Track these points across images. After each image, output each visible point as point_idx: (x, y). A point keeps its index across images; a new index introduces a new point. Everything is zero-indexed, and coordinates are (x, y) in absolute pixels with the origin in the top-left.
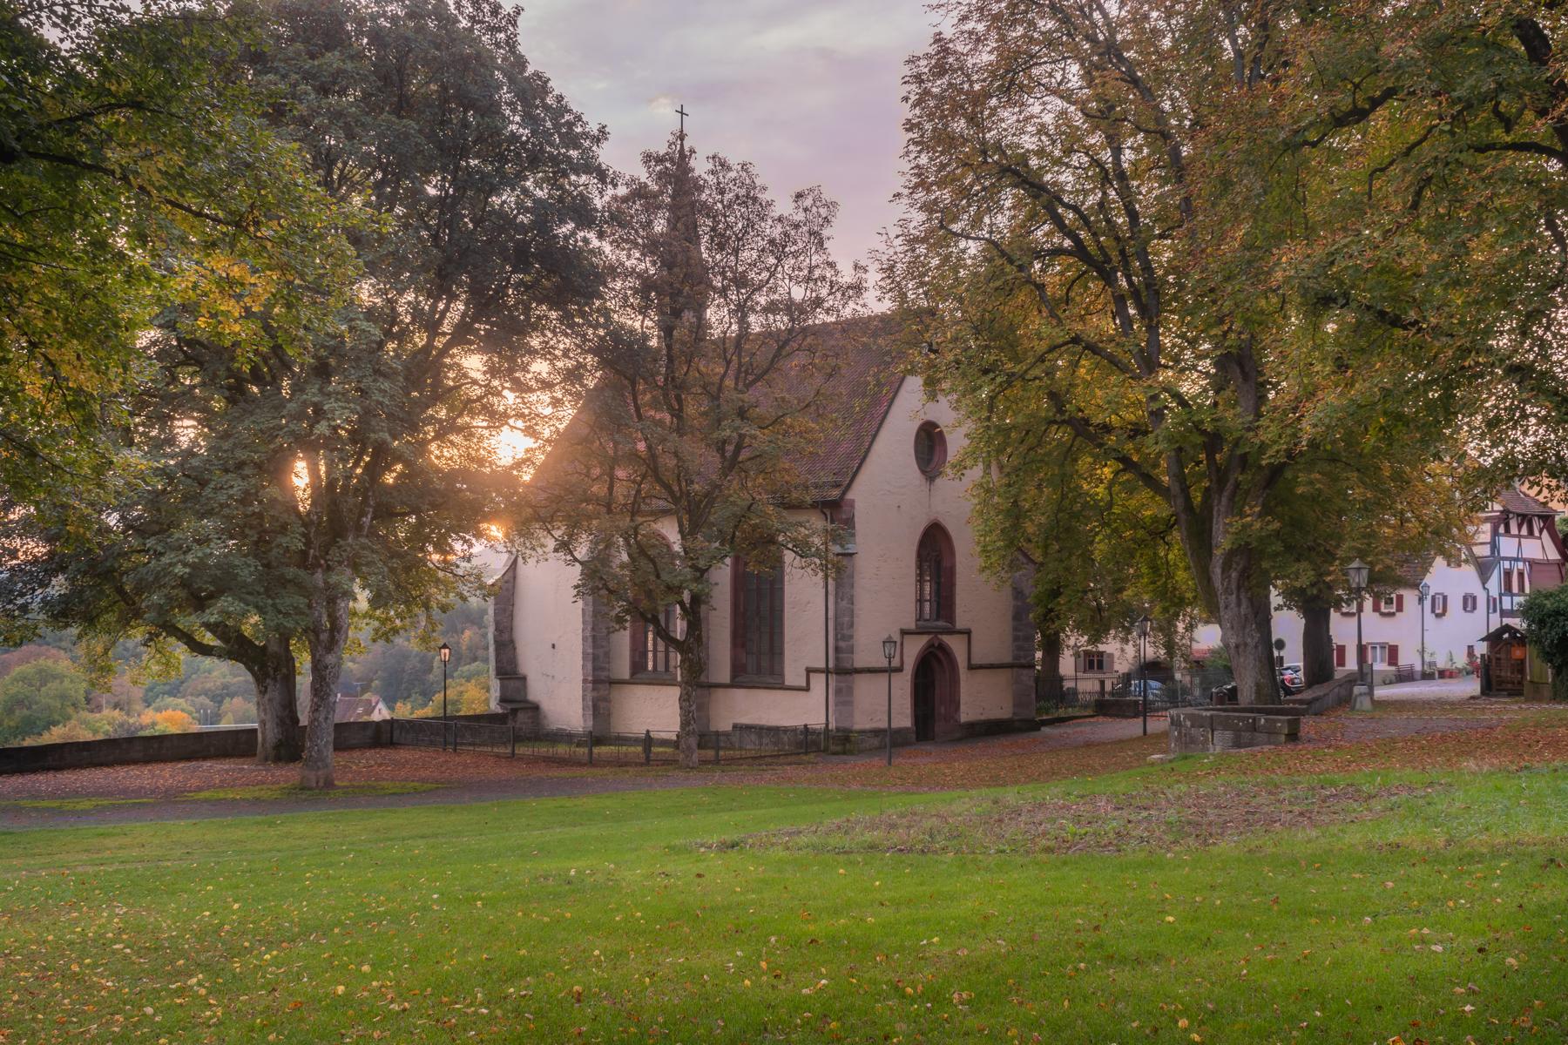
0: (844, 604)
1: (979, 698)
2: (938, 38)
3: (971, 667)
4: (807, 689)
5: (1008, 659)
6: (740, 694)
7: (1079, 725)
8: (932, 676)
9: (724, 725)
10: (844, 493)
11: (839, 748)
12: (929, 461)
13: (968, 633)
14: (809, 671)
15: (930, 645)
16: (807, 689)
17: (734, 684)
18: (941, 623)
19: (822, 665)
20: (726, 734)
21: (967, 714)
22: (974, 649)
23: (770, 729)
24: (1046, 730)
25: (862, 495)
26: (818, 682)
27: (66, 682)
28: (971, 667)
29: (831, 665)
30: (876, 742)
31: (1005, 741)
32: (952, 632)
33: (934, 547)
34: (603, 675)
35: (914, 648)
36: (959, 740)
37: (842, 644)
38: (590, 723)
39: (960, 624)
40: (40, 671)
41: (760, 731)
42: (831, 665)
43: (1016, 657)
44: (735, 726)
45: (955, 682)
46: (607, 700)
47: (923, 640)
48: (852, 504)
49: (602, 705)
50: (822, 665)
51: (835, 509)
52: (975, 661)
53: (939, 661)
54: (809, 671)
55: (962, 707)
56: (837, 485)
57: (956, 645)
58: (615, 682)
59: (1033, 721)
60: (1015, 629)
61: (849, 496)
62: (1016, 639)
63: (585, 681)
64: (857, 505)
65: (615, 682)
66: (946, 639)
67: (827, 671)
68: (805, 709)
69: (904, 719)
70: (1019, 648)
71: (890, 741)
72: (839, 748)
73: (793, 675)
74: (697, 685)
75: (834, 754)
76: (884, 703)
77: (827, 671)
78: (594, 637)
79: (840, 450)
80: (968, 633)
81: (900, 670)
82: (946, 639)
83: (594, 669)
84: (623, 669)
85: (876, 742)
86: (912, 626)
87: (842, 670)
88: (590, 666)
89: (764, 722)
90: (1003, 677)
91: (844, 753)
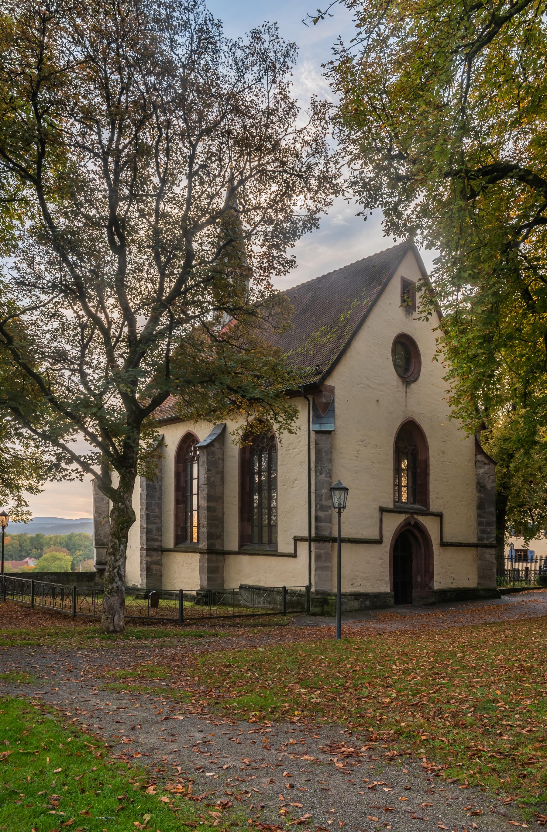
0: (322, 477)
1: (450, 570)
2: (426, 249)
3: (443, 544)
4: (295, 556)
5: (473, 540)
6: (245, 559)
7: (532, 595)
8: (409, 551)
9: (233, 583)
10: (324, 378)
11: (318, 610)
12: (406, 370)
13: (440, 516)
14: (297, 540)
15: (407, 523)
16: (295, 556)
17: (241, 552)
18: (416, 506)
19: (306, 534)
20: (234, 593)
21: (441, 581)
22: (445, 530)
23: (265, 589)
24: (505, 598)
25: (340, 382)
26: (303, 548)
27: (63, 562)
28: (443, 544)
29: (313, 535)
30: (356, 604)
31: (473, 606)
32: (427, 513)
33: (410, 441)
34: (156, 544)
35: (392, 524)
36: (433, 604)
37: (321, 514)
38: (205, 583)
39: (433, 508)
40: (53, 557)
41: (257, 591)
42: (313, 535)
43: (480, 539)
44: (242, 587)
45: (429, 555)
46: (159, 563)
47: (401, 518)
48: (332, 390)
49: (155, 567)
50: (306, 534)
51: (316, 394)
52: (446, 539)
53: (416, 538)
54: (297, 540)
55: (436, 577)
56: (318, 373)
57: (430, 525)
58: (164, 551)
59: (494, 590)
60: (479, 516)
61: (329, 382)
62: (480, 524)
63: (142, 549)
64: (337, 392)
65: (164, 551)
66: (421, 519)
67: (310, 540)
68: (290, 573)
69: (384, 586)
70: (482, 531)
71: (370, 604)
72: (318, 610)
73: (284, 544)
74: (215, 555)
75: (314, 614)
76: (367, 571)
77: (310, 540)
78: (147, 515)
79: (325, 351)
80: (440, 516)
81: (379, 542)
82: (421, 519)
83: (147, 540)
84: (169, 541)
85: (356, 604)
86: (391, 506)
87: (323, 539)
88: (144, 536)
89: (262, 584)
90: (470, 555)
91: (323, 614)
